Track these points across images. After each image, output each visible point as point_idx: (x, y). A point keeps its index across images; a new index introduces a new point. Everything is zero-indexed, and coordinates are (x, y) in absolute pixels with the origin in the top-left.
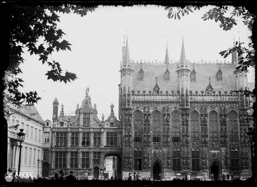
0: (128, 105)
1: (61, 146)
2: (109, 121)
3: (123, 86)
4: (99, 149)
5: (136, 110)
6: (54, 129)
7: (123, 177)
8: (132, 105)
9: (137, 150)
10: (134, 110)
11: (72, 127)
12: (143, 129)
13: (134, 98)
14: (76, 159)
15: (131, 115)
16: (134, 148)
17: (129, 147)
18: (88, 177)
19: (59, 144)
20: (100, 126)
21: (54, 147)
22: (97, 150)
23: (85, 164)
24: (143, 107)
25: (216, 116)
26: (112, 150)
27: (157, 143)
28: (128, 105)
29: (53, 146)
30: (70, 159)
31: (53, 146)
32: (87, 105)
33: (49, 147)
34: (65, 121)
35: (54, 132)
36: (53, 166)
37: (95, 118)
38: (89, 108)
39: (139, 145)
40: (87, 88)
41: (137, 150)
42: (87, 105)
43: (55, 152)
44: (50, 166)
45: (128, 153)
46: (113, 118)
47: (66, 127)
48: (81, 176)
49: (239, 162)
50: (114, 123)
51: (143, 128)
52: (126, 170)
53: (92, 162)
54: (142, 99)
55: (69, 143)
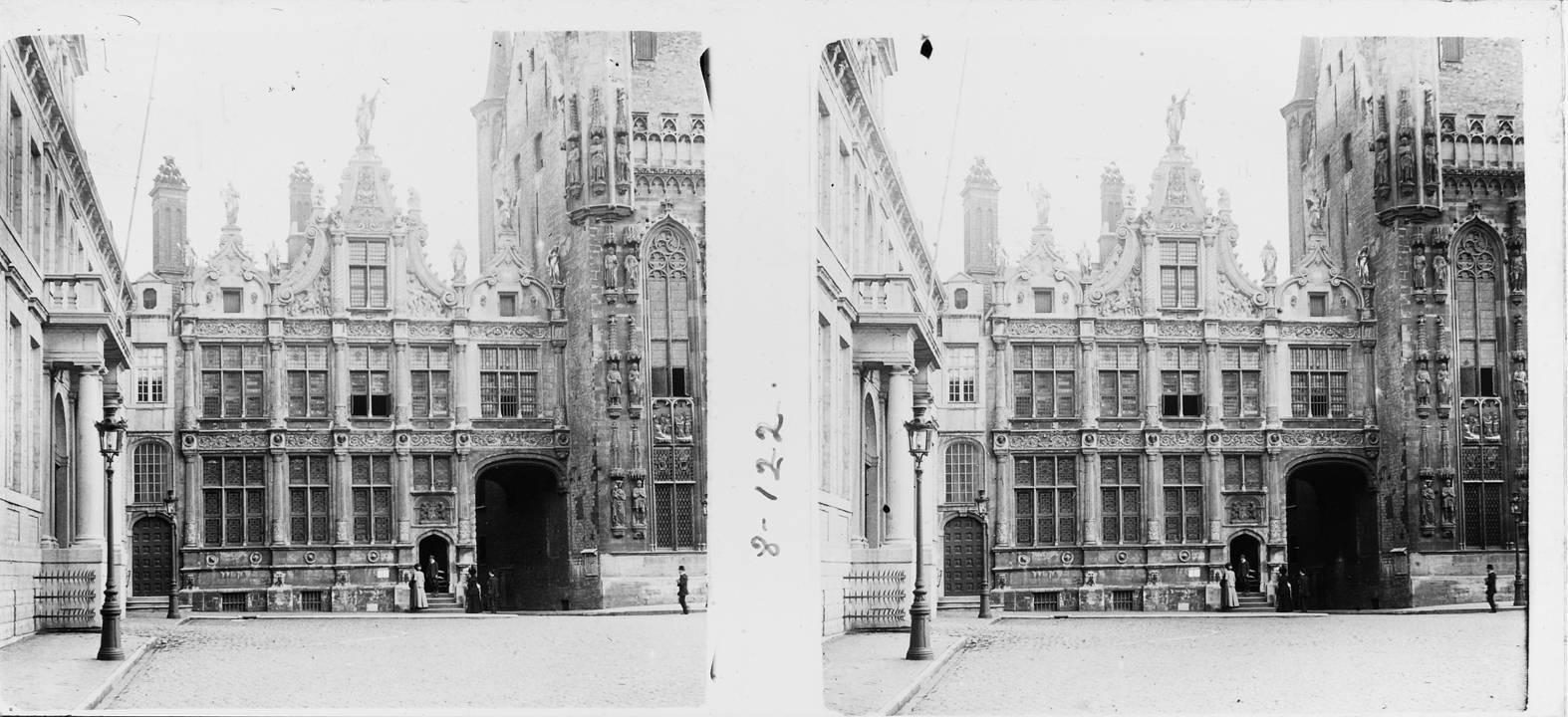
0: (1430, 191)
1: (236, 424)
2: (1300, 287)
3: (1397, 88)
4: (446, 438)
5: (1466, 221)
6: (190, 326)
7: (1414, 587)
8: (1443, 192)
9: (1477, 437)
10: (1456, 221)
11: (290, 314)
12: (1507, 323)
13: (1454, 154)
14: (323, 495)
15: (1443, 245)
16: (1465, 430)
17: (631, 422)
18: (393, 590)
19: (220, 413)
20: (446, 308)
21: (1010, 427)
22: (1245, 444)
23: (373, 521)
24: (692, 203)
25: (1492, 250)
26: (513, 444)
27: (1482, 400)
28: (1430, 191)
29: (192, 425)
30: (288, 492)
31: (192, 425)
32: (370, 193)
33: (167, 429)
34: (253, 283)
35: (192, 343)
36: (196, 537)
37: (1229, 265)
38: (1191, 209)
39: (1486, 408)
40: (1174, 99)
41: (1477, 437)
42: (370, 193)
43: (1012, 457)
44: (990, 532)
45: (1434, 456)
46: (1324, 267)
47: (261, 315)
48: (355, 586)
49: (1512, 503)
50: (521, 295)
51: (1504, 318)
52: (616, 545)
53: (1220, 507)
54: (689, 162)
55: (279, 404)
